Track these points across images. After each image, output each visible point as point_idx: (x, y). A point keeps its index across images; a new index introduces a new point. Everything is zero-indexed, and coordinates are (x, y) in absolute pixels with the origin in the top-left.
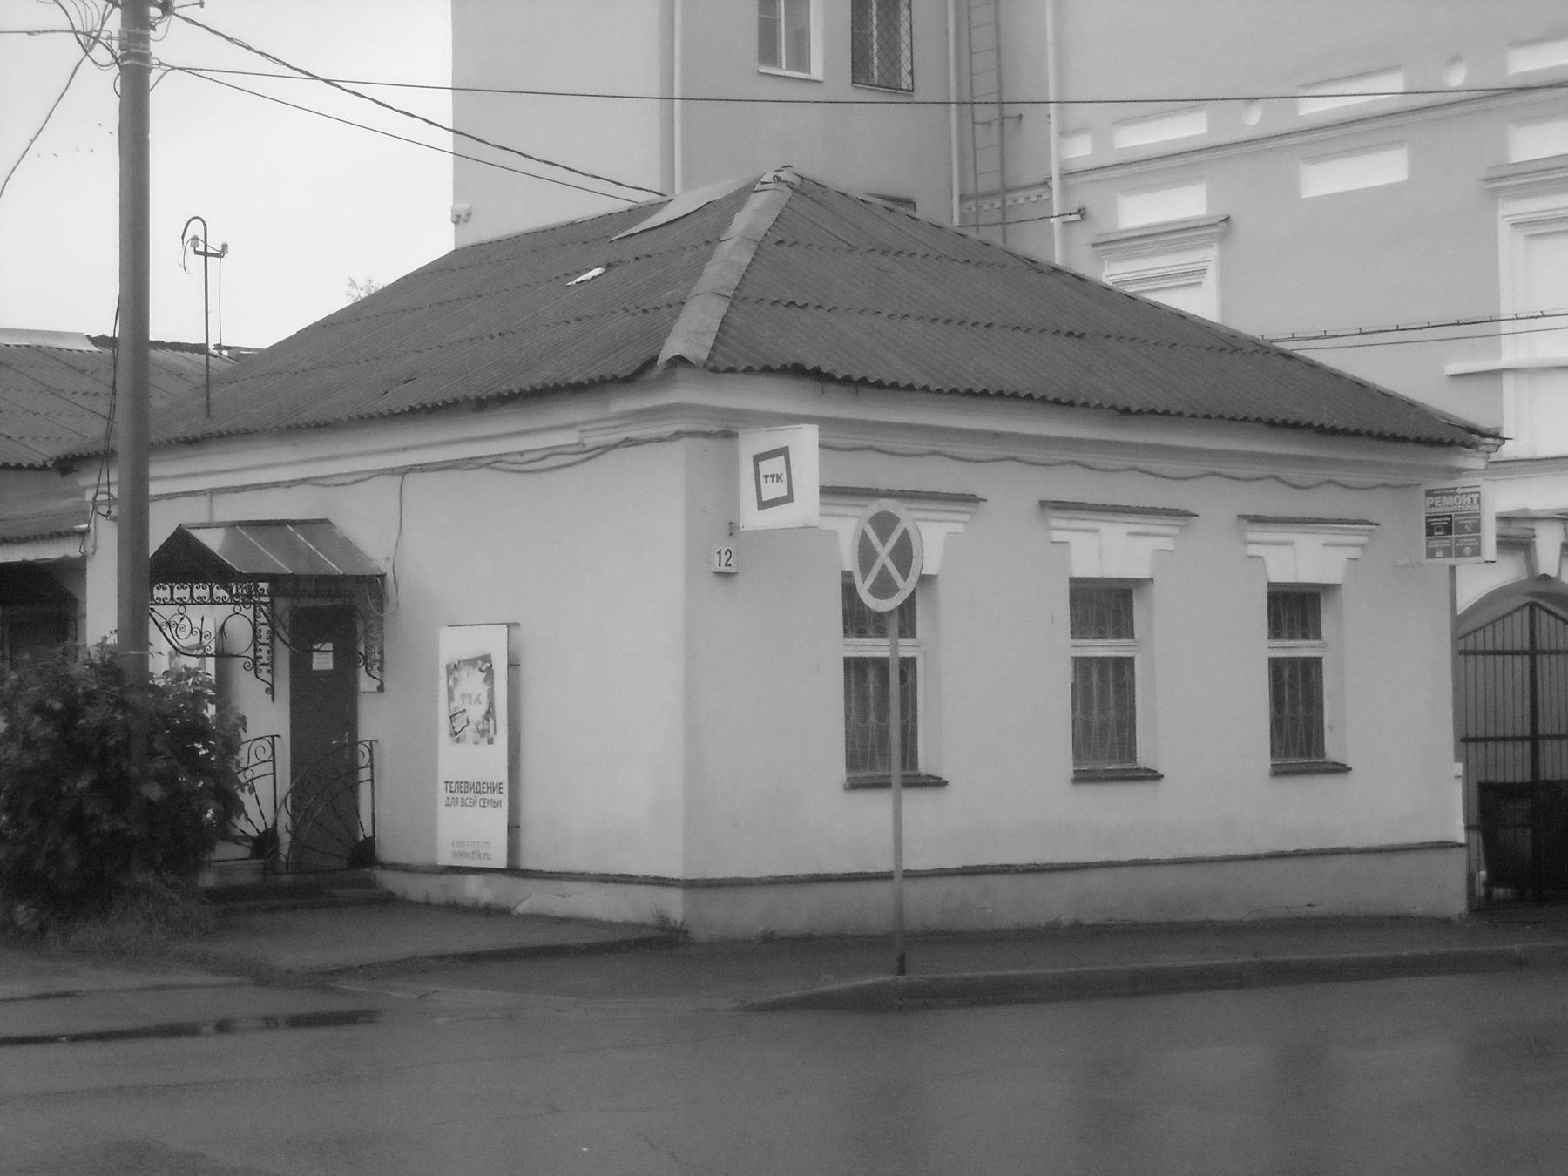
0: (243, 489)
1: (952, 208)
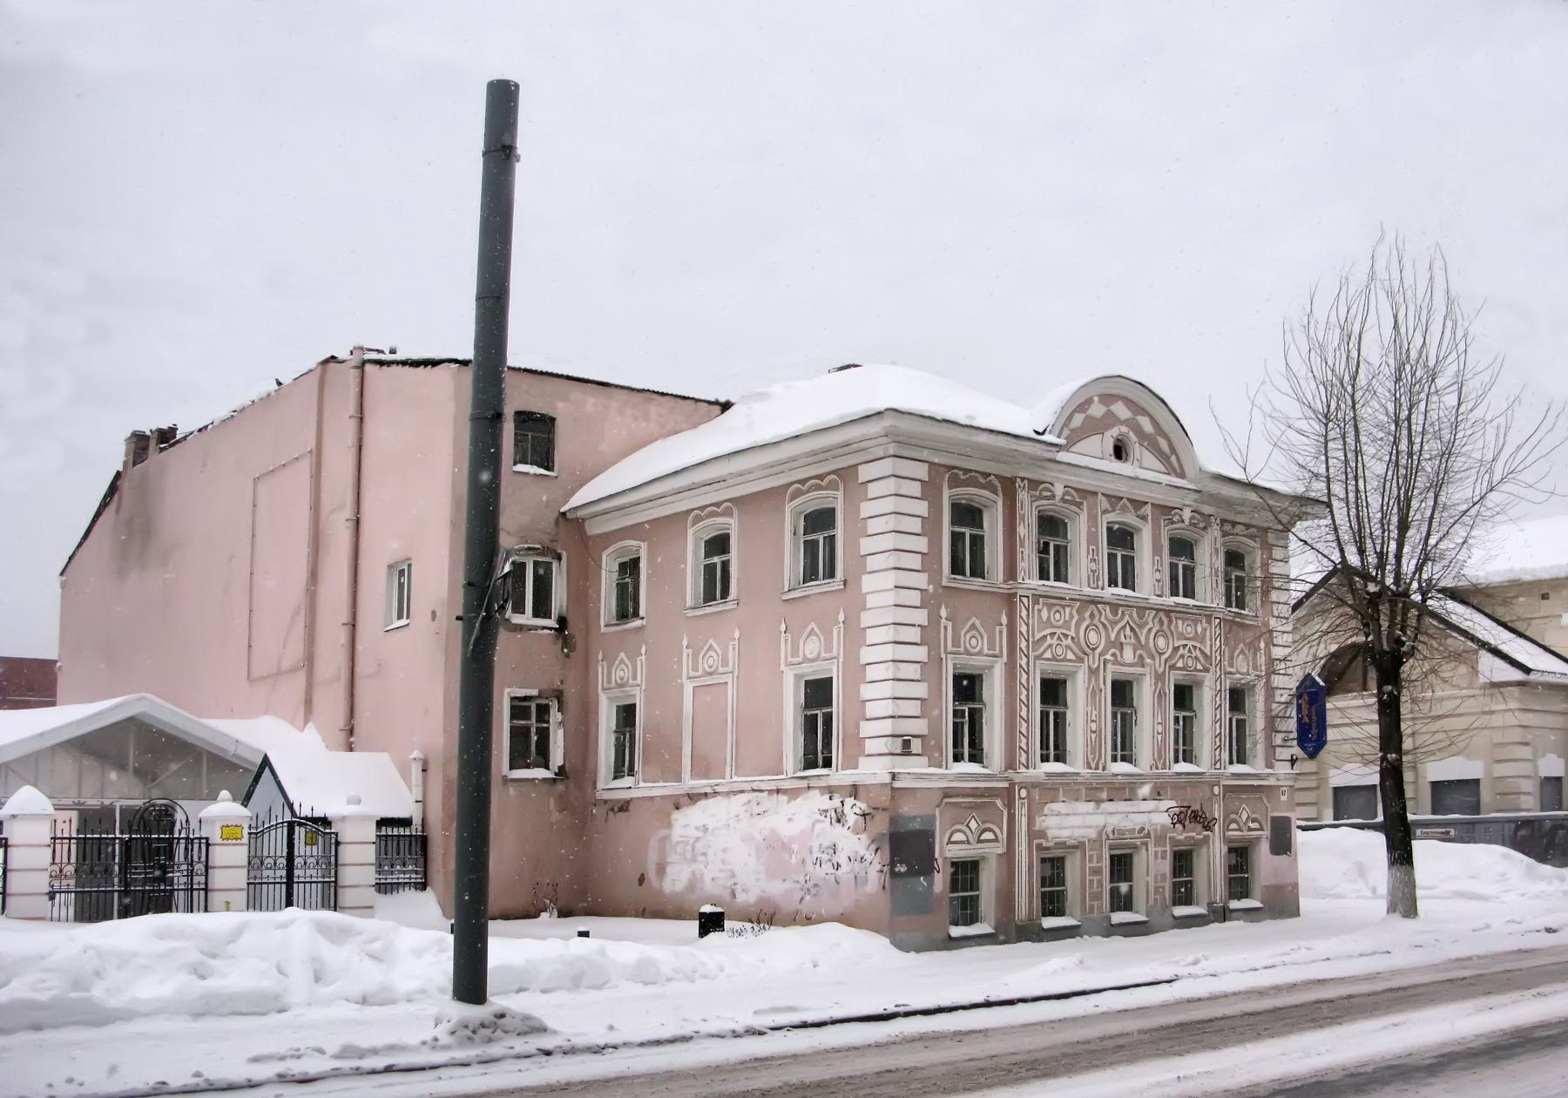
0: (314, 575)
1: (692, 663)
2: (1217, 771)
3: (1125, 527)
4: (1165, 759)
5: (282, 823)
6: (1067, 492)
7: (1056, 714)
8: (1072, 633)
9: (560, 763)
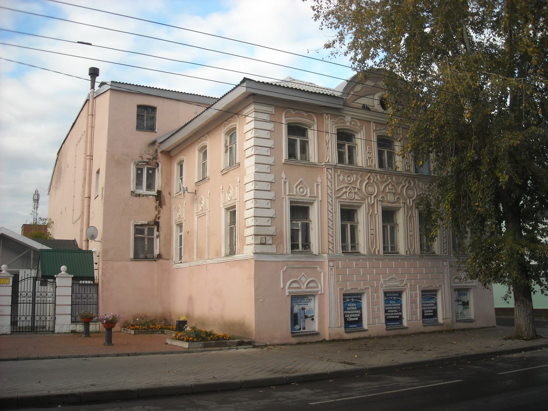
2: (445, 254)
3: (382, 137)
4: (414, 249)
5: (31, 277)
6: (352, 120)
7: (351, 226)
8: (358, 187)
9: (158, 253)
